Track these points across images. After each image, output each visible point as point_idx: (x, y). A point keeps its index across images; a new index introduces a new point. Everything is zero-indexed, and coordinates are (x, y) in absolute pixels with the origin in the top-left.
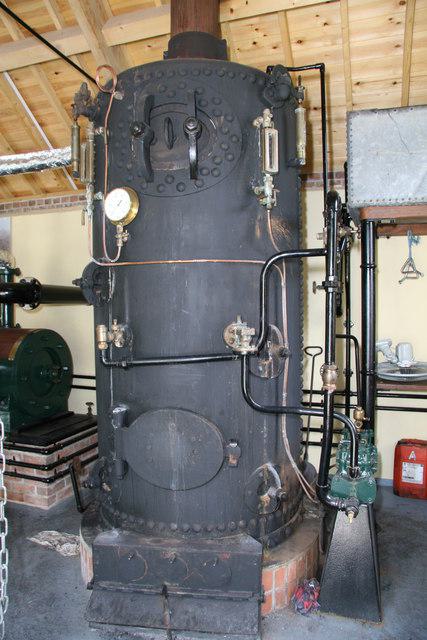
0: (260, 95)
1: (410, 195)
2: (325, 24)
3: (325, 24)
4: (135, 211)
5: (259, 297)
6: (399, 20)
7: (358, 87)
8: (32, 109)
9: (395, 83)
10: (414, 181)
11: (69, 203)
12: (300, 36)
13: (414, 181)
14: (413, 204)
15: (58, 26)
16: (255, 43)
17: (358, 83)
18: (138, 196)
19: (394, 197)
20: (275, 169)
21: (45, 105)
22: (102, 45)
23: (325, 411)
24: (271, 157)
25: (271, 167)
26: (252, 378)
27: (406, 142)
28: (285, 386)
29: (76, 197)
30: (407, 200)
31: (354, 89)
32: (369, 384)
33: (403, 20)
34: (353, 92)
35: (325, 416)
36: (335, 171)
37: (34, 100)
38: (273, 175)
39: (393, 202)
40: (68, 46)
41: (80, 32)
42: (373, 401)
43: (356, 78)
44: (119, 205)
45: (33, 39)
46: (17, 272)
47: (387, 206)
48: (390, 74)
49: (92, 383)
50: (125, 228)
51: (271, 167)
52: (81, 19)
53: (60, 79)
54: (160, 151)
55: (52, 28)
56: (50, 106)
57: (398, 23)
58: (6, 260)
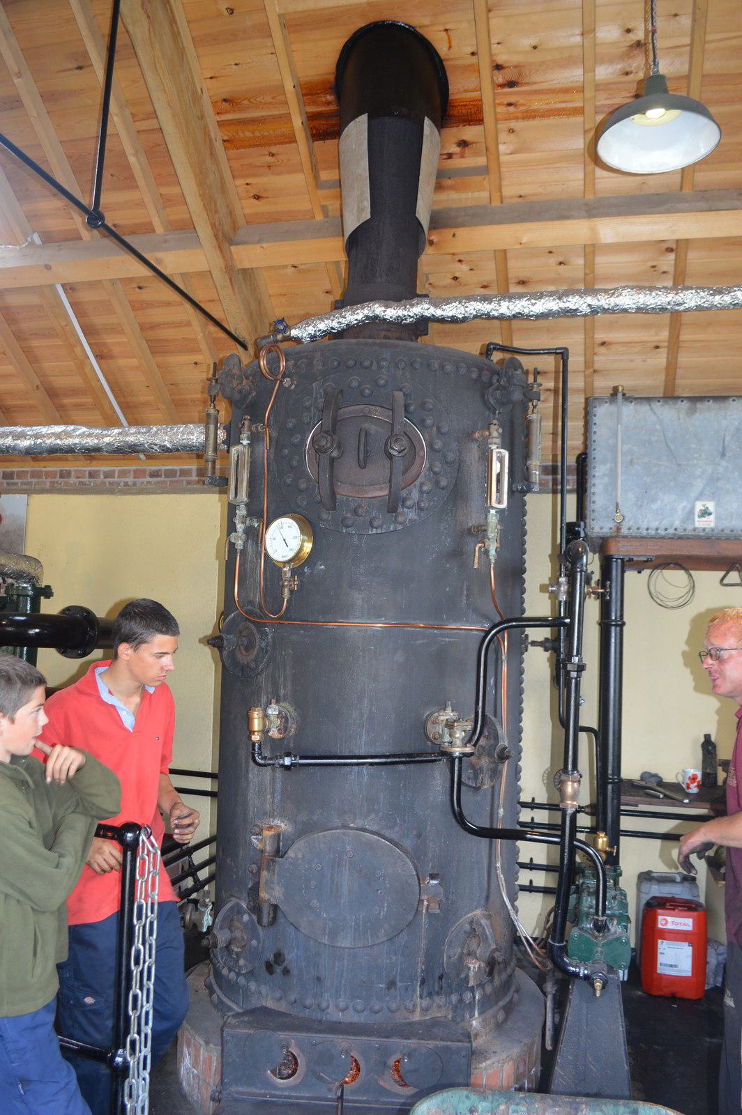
0: (483, 396)
1: (677, 523)
2: (560, 263)
3: (560, 263)
4: (308, 547)
5: (475, 668)
6: (665, 269)
7: (602, 349)
8: (88, 331)
9: (657, 347)
10: (681, 506)
11: (130, 480)
12: (523, 275)
13: (681, 506)
14: (680, 538)
15: (159, 229)
16: (455, 278)
17: (603, 344)
18: (308, 525)
19: (654, 524)
20: (504, 505)
21: (116, 330)
22: (229, 269)
23: (562, 836)
24: (498, 491)
25: (500, 502)
26: (463, 788)
27: (672, 447)
28: (501, 801)
29: (144, 471)
30: (671, 531)
31: (596, 351)
32: (614, 794)
33: (671, 270)
34: (595, 354)
35: (562, 844)
36: (551, 398)
37: (98, 320)
38: (500, 512)
39: (652, 532)
40: (171, 262)
41: (197, 242)
42: (617, 822)
43: (600, 336)
44: (284, 539)
45: (109, 243)
46: (47, 592)
47: (643, 537)
48: (650, 336)
49: (206, 784)
50: (293, 572)
51: (500, 502)
52: (204, 231)
53: (145, 295)
54: (348, 466)
55: (148, 229)
56: (122, 332)
57: (664, 272)
58: (33, 573)
